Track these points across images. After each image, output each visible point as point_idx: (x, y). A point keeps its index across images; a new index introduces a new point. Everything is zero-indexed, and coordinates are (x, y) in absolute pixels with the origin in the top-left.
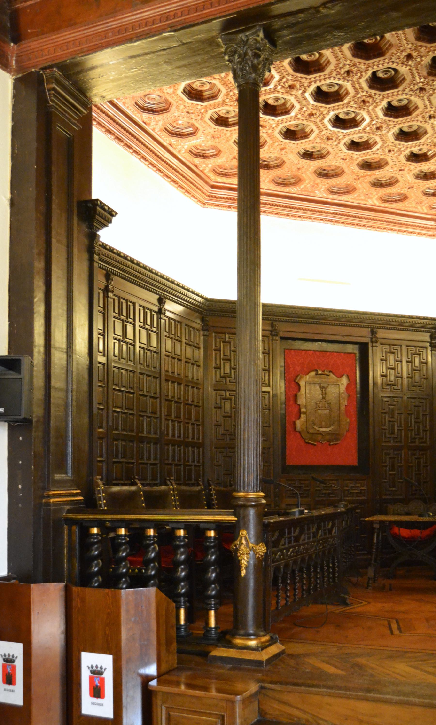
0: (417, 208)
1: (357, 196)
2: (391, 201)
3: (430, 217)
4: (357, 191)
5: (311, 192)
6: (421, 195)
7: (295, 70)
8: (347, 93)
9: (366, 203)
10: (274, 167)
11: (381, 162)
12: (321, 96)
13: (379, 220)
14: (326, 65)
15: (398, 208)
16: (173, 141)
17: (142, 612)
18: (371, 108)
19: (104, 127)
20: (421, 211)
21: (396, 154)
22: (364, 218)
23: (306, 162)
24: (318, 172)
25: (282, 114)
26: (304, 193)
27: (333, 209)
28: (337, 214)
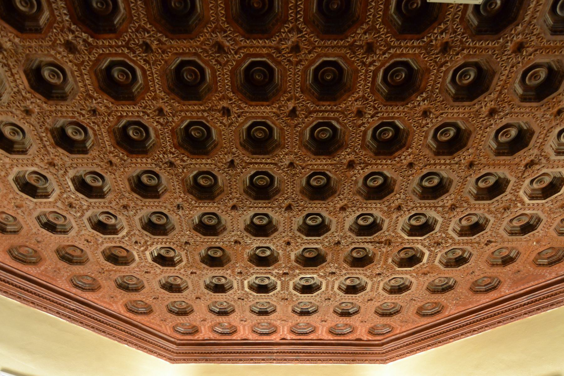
0: (161, 326)
1: (102, 297)
2: (137, 313)
3: (173, 340)
4: (101, 289)
5: (53, 279)
6: (165, 310)
7: (77, 189)
8: (134, 260)
9: (111, 308)
10: (11, 232)
11: (128, 259)
12: (82, 186)
13: (121, 330)
15: (142, 322)
17: (470, 303)
20: (165, 332)
21: (142, 248)
22: (106, 323)
25: (42, 197)
26: (44, 278)
27: (73, 305)
28: (77, 311)
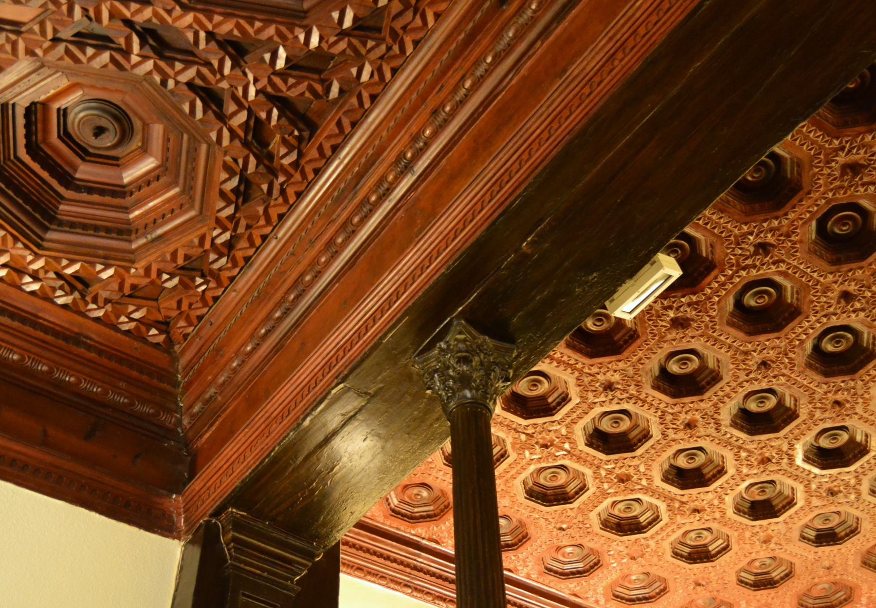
7: (751, 433)
10: (782, 579)
14: (867, 442)
16: (572, 586)
18: (859, 409)
19: (428, 593)
23: (827, 551)
24: (812, 534)
